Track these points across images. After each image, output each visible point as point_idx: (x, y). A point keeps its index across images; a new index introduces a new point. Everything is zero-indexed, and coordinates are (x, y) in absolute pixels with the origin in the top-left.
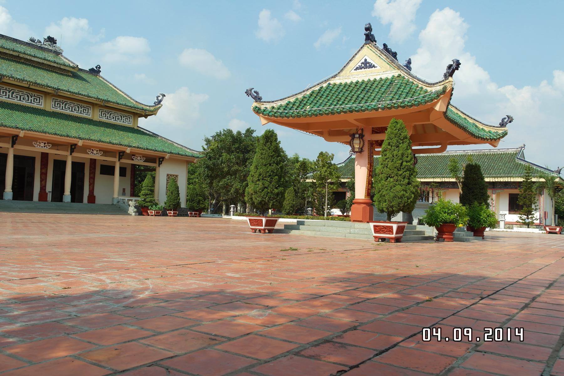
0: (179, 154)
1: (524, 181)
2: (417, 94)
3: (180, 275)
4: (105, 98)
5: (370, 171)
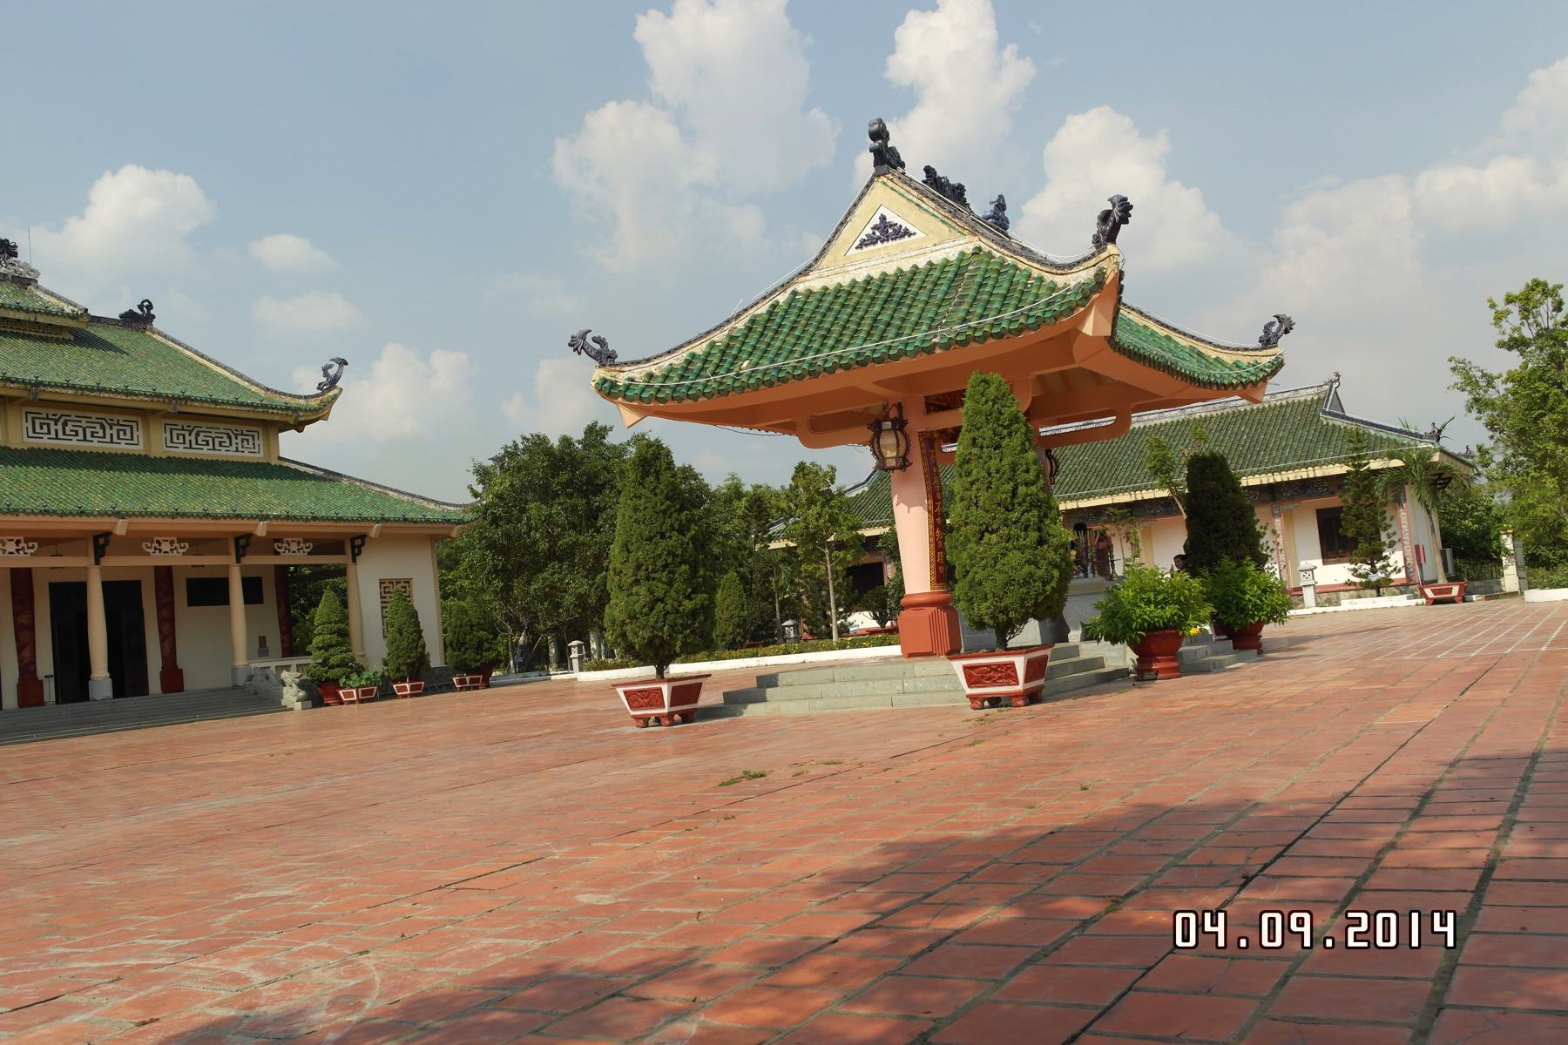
0: (406, 520)
1: (1349, 473)
2: (1031, 298)
3: (452, 922)
4: (177, 392)
5: (936, 516)
